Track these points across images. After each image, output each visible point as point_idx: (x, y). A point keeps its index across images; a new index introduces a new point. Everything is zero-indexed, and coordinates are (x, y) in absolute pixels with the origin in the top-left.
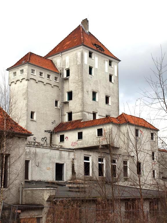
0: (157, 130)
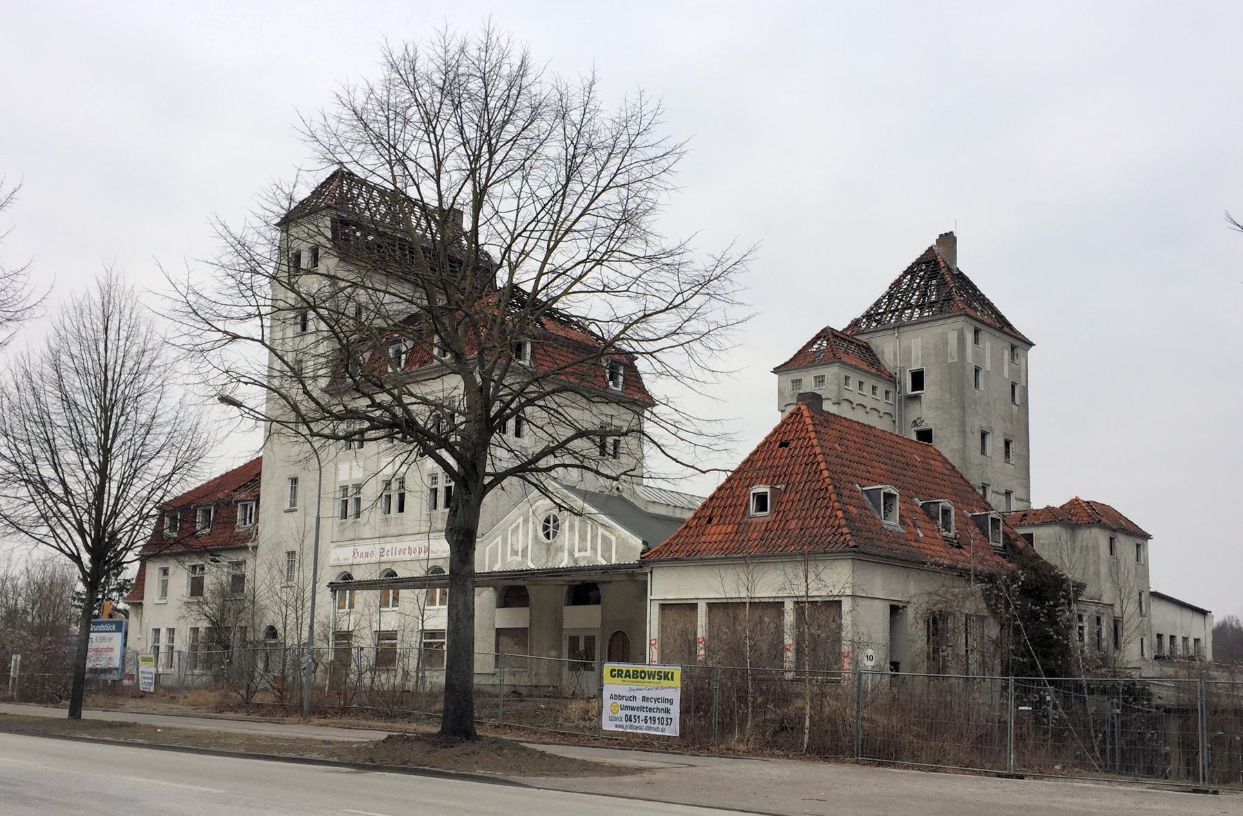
0: (1146, 537)
